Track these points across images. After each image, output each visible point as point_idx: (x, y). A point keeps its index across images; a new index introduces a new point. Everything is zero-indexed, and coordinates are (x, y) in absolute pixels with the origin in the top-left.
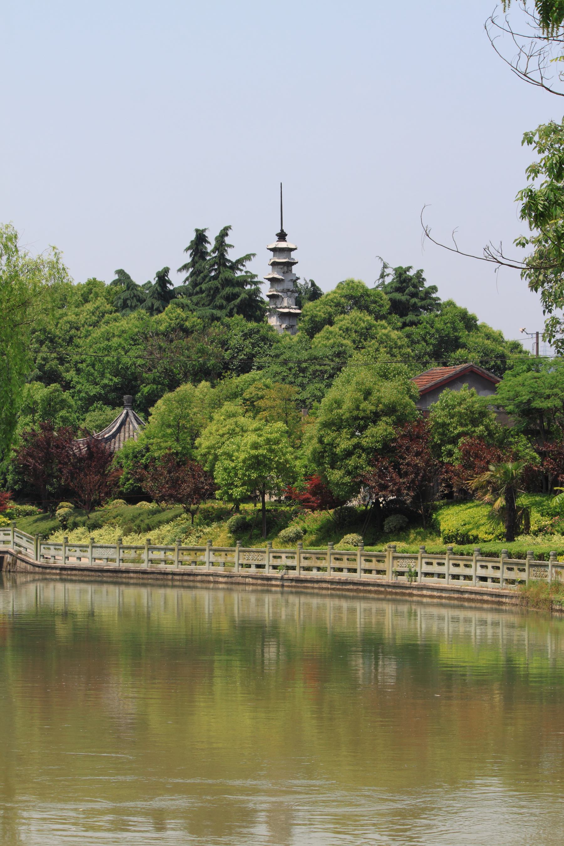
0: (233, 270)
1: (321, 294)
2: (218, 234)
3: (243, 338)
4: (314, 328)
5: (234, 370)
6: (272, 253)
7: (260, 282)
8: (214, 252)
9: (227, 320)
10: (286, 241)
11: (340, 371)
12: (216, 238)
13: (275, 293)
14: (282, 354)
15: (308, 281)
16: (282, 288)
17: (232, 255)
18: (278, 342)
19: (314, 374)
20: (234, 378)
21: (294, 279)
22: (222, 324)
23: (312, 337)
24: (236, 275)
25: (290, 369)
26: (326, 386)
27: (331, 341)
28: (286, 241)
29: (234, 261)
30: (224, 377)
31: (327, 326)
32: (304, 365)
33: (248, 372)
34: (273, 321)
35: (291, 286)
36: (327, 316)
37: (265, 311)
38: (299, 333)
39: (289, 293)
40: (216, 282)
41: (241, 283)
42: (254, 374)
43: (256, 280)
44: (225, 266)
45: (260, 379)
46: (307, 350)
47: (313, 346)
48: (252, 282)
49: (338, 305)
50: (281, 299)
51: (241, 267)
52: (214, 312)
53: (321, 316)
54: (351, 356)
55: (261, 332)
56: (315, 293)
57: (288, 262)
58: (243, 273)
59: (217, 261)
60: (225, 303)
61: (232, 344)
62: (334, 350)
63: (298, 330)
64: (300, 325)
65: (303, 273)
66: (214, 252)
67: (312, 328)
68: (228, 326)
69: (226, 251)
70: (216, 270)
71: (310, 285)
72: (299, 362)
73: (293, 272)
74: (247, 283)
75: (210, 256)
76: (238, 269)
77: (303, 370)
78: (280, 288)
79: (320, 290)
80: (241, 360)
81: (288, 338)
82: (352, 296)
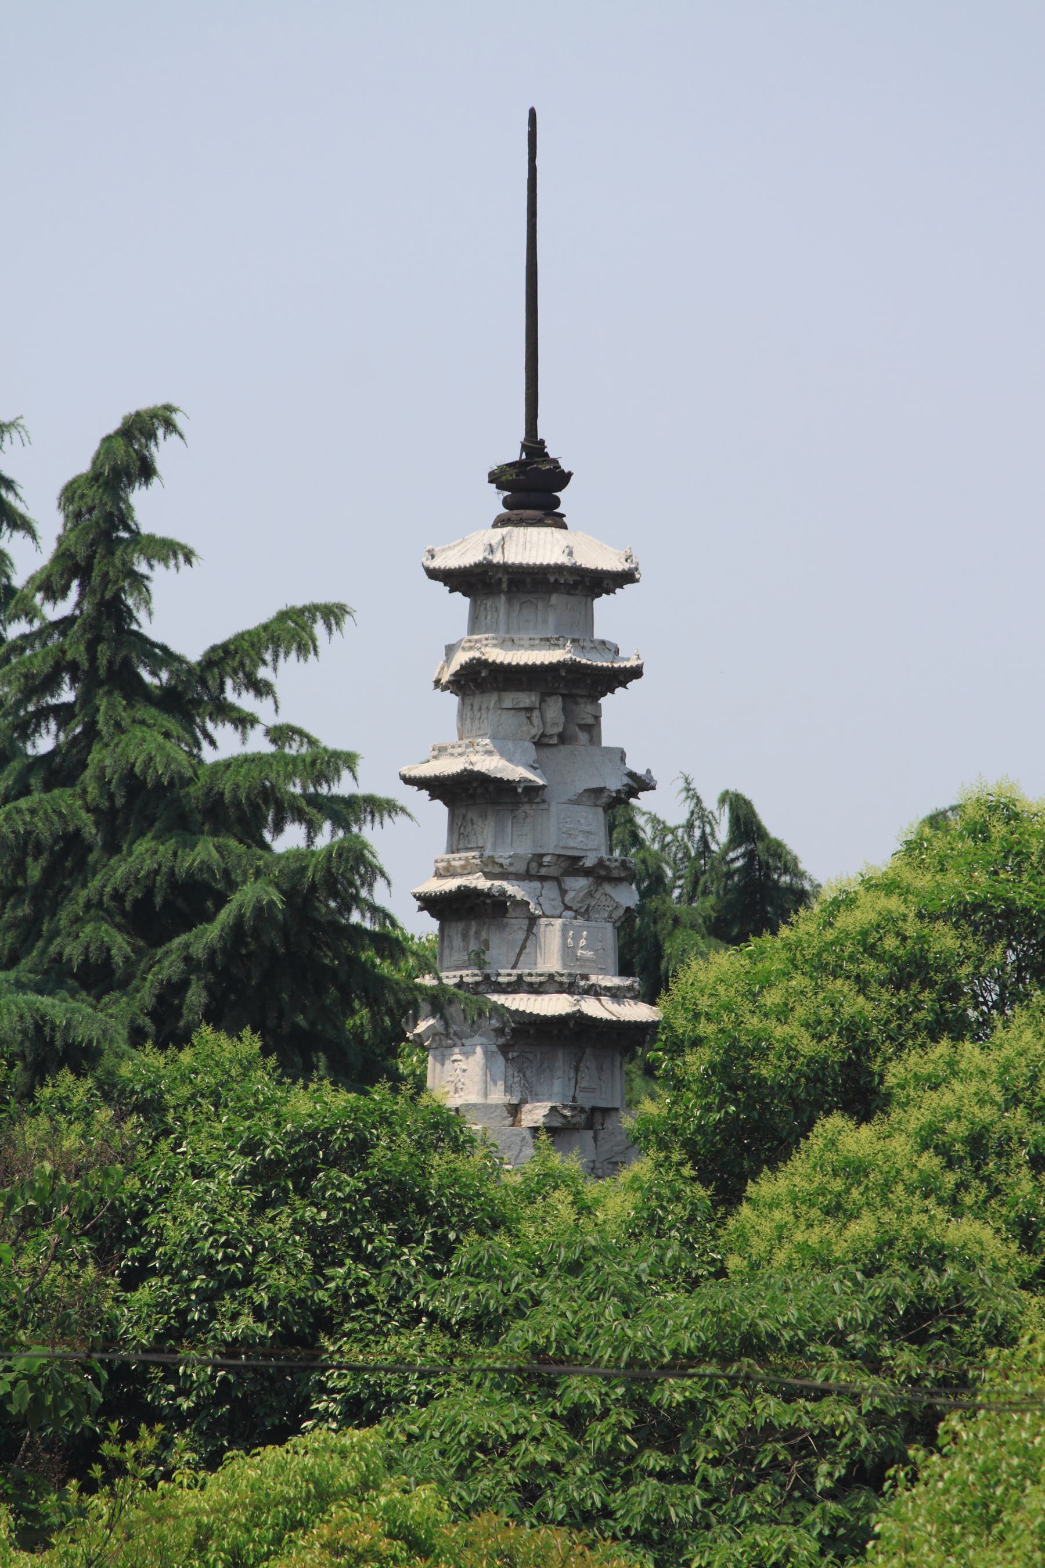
0: (188, 721)
1: (801, 897)
2: (83, 465)
3: (251, 1196)
4: (746, 1134)
5: (180, 1420)
6: (461, 603)
7: (378, 807)
8: (53, 591)
9: (141, 1065)
10: (559, 522)
11: (931, 1444)
12: (70, 494)
13: (481, 883)
14: (518, 1311)
15: (710, 803)
16: (524, 848)
17: (181, 617)
18: (498, 1223)
19: (745, 1458)
20: (182, 1476)
21: (615, 783)
22: (109, 1090)
23: (730, 1195)
24: (209, 755)
25: (575, 1420)
26: (827, 1542)
27: (863, 1228)
28: (559, 522)
29: (193, 652)
30: (116, 1469)
31: (834, 1123)
32: (673, 1392)
33: (279, 1437)
34: (463, 1080)
35: (586, 836)
36: (832, 1049)
37: (408, 1004)
38: (642, 1167)
39: (577, 885)
40: (64, 798)
41: (246, 807)
42: (322, 1448)
43: (344, 786)
44: (134, 690)
45: (367, 1484)
46: (694, 1283)
47: (734, 1262)
48: (314, 800)
49: (913, 970)
50: (517, 924)
51: (246, 701)
52: (56, 1007)
53: (791, 1051)
54: (1001, 1336)
55: (377, 1155)
56: (756, 889)
57: (572, 668)
58: (258, 743)
59: (77, 652)
60: (120, 945)
61: (174, 1234)
62: (879, 1286)
63: (637, 1142)
64: (649, 1107)
65: (678, 743)
66: (51, 586)
67: (730, 1128)
68: (151, 1108)
69: (139, 581)
70: (64, 714)
71: (722, 833)
72: (640, 1373)
73: (609, 738)
74: (287, 809)
75: (31, 613)
76: (224, 711)
77: (667, 1430)
78: (514, 845)
79: (791, 867)
80: (232, 1348)
81: (561, 1199)
82: (1011, 912)
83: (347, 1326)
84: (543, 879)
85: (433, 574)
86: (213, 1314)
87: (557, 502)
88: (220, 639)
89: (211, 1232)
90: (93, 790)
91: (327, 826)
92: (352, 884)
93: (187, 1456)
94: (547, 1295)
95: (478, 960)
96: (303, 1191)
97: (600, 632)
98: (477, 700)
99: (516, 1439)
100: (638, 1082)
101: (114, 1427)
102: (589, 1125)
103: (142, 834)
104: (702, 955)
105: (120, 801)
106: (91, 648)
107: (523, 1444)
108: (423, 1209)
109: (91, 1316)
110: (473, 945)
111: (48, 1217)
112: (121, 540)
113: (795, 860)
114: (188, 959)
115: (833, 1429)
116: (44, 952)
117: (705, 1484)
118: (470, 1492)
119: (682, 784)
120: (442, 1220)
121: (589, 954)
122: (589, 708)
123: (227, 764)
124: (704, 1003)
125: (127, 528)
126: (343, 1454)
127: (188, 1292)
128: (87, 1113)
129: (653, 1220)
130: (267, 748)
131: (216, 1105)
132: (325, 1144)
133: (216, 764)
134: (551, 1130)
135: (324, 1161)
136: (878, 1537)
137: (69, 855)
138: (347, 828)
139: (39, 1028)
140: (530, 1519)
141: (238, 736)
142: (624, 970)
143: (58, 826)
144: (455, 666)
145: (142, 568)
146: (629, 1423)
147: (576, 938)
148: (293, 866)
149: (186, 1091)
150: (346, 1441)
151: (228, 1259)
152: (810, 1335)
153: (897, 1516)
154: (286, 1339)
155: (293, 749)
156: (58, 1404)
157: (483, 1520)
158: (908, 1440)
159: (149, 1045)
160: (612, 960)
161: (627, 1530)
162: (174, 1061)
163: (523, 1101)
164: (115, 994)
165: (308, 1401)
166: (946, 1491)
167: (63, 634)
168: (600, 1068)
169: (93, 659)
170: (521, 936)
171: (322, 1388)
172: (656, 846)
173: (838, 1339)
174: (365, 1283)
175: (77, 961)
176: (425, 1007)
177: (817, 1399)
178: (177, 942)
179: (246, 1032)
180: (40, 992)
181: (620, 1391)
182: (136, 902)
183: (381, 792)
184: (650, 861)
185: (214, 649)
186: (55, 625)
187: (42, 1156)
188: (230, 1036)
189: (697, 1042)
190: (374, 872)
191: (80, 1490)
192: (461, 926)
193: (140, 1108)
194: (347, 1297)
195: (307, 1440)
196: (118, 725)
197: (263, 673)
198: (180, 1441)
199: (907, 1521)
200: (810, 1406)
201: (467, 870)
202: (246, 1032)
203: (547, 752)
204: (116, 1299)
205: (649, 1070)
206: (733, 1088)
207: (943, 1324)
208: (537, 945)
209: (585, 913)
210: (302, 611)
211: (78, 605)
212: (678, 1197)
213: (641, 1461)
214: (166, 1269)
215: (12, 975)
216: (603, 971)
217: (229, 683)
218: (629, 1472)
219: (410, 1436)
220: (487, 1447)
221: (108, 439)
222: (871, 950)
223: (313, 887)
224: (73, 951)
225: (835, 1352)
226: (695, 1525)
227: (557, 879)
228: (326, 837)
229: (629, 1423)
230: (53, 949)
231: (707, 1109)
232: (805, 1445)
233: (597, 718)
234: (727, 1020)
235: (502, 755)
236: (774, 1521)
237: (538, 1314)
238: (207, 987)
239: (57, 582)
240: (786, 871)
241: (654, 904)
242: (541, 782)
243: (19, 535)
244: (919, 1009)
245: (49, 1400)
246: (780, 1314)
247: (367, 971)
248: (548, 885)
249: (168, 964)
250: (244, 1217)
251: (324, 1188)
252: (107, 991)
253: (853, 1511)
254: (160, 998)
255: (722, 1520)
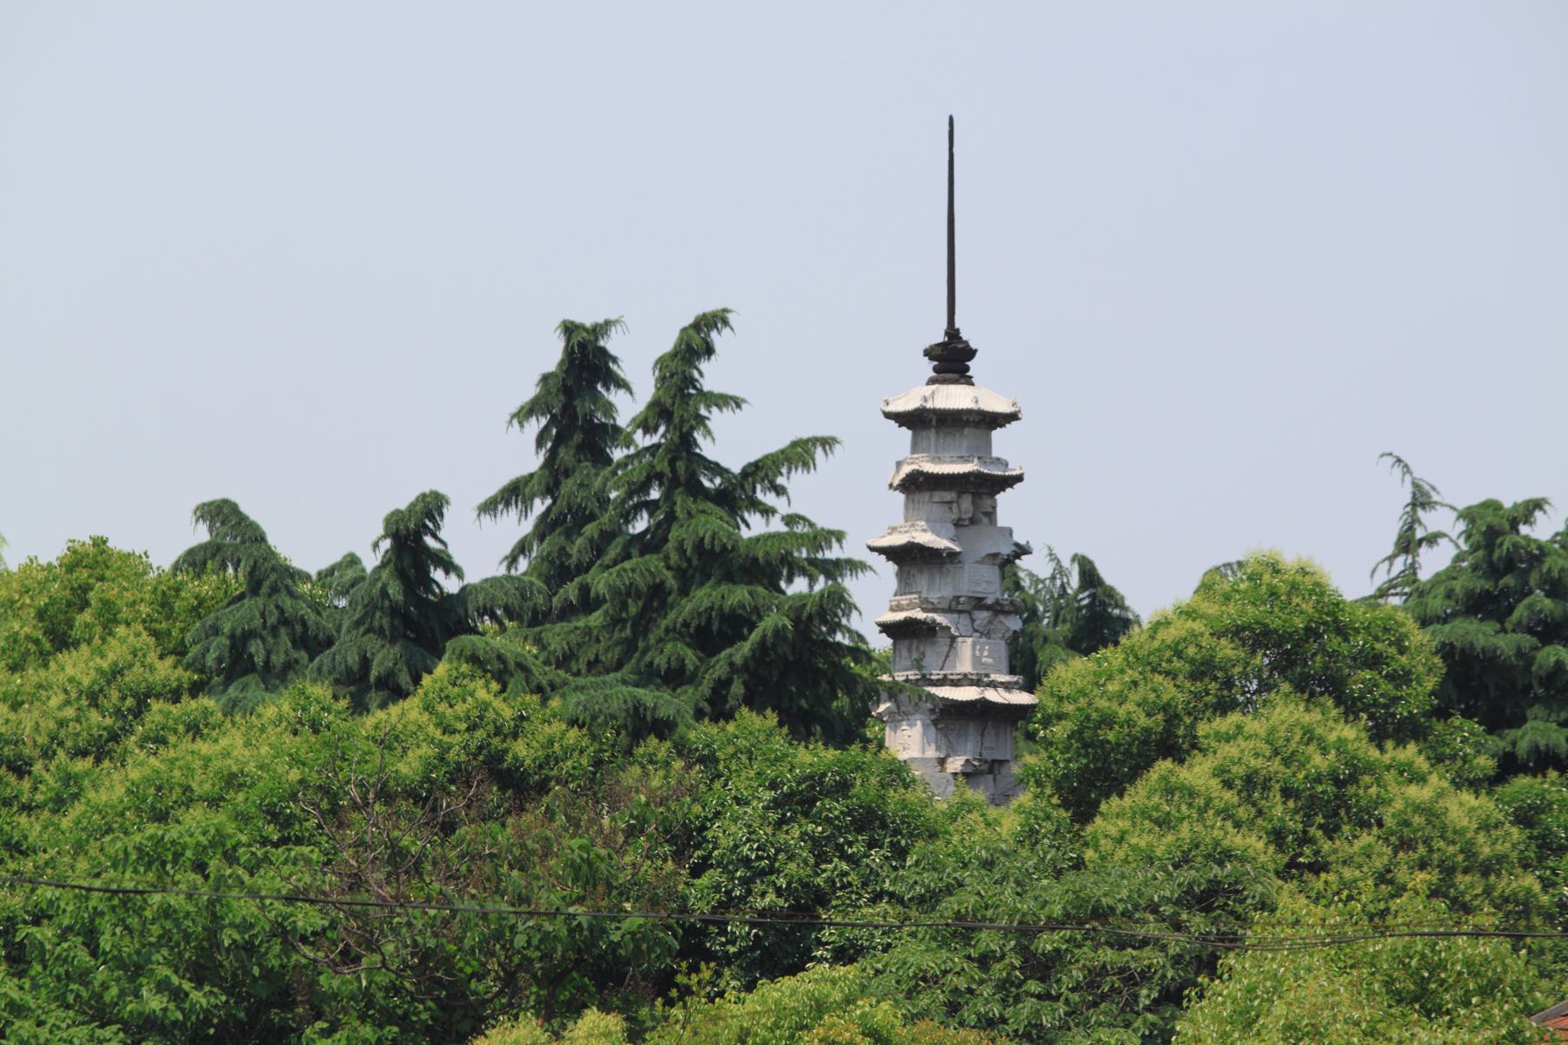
1: (1126, 624)
3: (773, 816)
5: (727, 960)
6: (906, 434)
7: (855, 566)
9: (701, 733)
10: (969, 381)
11: (1213, 974)
12: (661, 363)
13: (920, 615)
14: (949, 890)
15: (1066, 563)
17: (728, 444)
18: (933, 835)
19: (1092, 985)
20: (731, 995)
21: (1006, 550)
22: (681, 749)
24: (745, 533)
25: (984, 961)
28: (969, 381)
29: (736, 469)
30: (686, 991)
32: (1046, 943)
33: (793, 970)
34: (908, 742)
35: (989, 585)
37: (873, 692)
38: (1025, 798)
40: (653, 561)
41: (765, 568)
43: (834, 553)
44: (696, 490)
45: (849, 1000)
48: (813, 562)
49: (1203, 669)
50: (943, 642)
51: (769, 499)
52: (647, 696)
53: (1130, 722)
55: (857, 789)
56: (1097, 618)
58: (776, 525)
59: (663, 466)
60: (690, 657)
63: (1021, 783)
64: (1030, 760)
65: (1047, 525)
66: (646, 425)
69: (701, 421)
70: (652, 507)
71: (1075, 581)
72: (1026, 931)
73: (1002, 520)
74: (794, 568)
75: (629, 442)
77: (1043, 967)
78: (941, 589)
80: (762, 913)
82: (1267, 632)
83: (834, 903)
84: (960, 612)
85: (888, 415)
86: (749, 892)
87: (968, 369)
88: (752, 459)
89: (748, 840)
90: (674, 558)
91: (822, 579)
92: (836, 615)
93: (733, 983)
94: (968, 881)
95: (918, 664)
96: (806, 814)
97: (995, 453)
98: (917, 497)
99: (945, 973)
100: (1022, 744)
101: (684, 965)
102: (991, 771)
103: (702, 584)
104: (1064, 661)
105: (695, 562)
106: (672, 463)
107: (949, 976)
108: (884, 826)
109: (671, 894)
110: (915, 655)
111: (642, 832)
112: (690, 395)
113: (1122, 598)
114: (731, 664)
115: (1149, 967)
116: (639, 661)
117: (1067, 1002)
118: (914, 1006)
119: (1046, 552)
120: (896, 832)
121: (990, 661)
122: (989, 502)
123: (758, 539)
124: (1066, 690)
125: (695, 387)
126: (834, 982)
127: (733, 879)
128: (667, 764)
129: (1033, 831)
130: (784, 529)
131: (750, 759)
132: (821, 783)
133: (750, 539)
134: (966, 775)
135: (820, 793)
136: (1179, 1033)
137: (656, 596)
138: (835, 579)
139: (636, 709)
140: (953, 1023)
141: (764, 521)
142: (1012, 671)
143: (649, 578)
144: (902, 475)
145: (703, 412)
146: (1017, 963)
147: (981, 651)
148: (798, 604)
149: (731, 750)
150: (835, 974)
151: (759, 858)
152: (1136, 907)
153: (1191, 1021)
154: (796, 908)
155: (800, 529)
156: (650, 950)
157: (922, 1025)
158: (1197, 974)
159: (706, 720)
160: (1004, 665)
161: (1016, 1031)
162: (723, 730)
163: (948, 756)
164: (685, 687)
165: (810, 950)
166: (1223, 1003)
167: (653, 455)
168: (997, 735)
169: (673, 470)
170: (946, 649)
171: (820, 943)
172: (1032, 591)
173: (1154, 908)
174: (846, 874)
175: (664, 666)
176: (884, 695)
177: (1139, 948)
178: (724, 654)
179: (769, 712)
180: (637, 686)
181: (1013, 943)
182: (699, 627)
183: (856, 557)
184: (1029, 601)
185: (750, 465)
186: (647, 449)
187: (637, 791)
188: (758, 713)
189: (1061, 717)
190: (851, 607)
191: (664, 1005)
192: (907, 642)
193: (702, 760)
194: (834, 883)
195: (810, 974)
196: (689, 513)
197: (780, 481)
198: (727, 972)
199: (1199, 1024)
200: (1135, 953)
201: (910, 607)
202: (769, 712)
203: (962, 530)
204: (687, 884)
205: (1031, 736)
206: (1086, 746)
207: (1221, 901)
208: (956, 655)
209: (986, 634)
210: (808, 441)
211: (663, 436)
212: (1048, 818)
213: (1024, 988)
214: (719, 864)
215: (619, 675)
216: (999, 672)
217: (759, 487)
218: (1018, 995)
219: (878, 972)
220: (925, 979)
221: (684, 330)
222: (1179, 654)
223: (810, 617)
224: (661, 661)
225: (1151, 918)
226: (1060, 1028)
227: (969, 612)
228: (821, 584)
229: (1017, 963)
230: (647, 659)
231: (1069, 760)
232: (1132, 977)
233: (994, 508)
234: (1083, 702)
235: (933, 532)
236: (1110, 1025)
237: (960, 894)
238: (745, 684)
239: (651, 422)
240: (1117, 606)
241: (1031, 628)
242: (958, 549)
243: (622, 392)
244: (1208, 694)
245: (644, 947)
246: (1112, 891)
247: (845, 671)
248: (963, 616)
249: (719, 667)
250: (769, 830)
251: (820, 812)
252: (680, 685)
253: (1163, 1019)
254: (714, 690)
255: (1077, 1025)
